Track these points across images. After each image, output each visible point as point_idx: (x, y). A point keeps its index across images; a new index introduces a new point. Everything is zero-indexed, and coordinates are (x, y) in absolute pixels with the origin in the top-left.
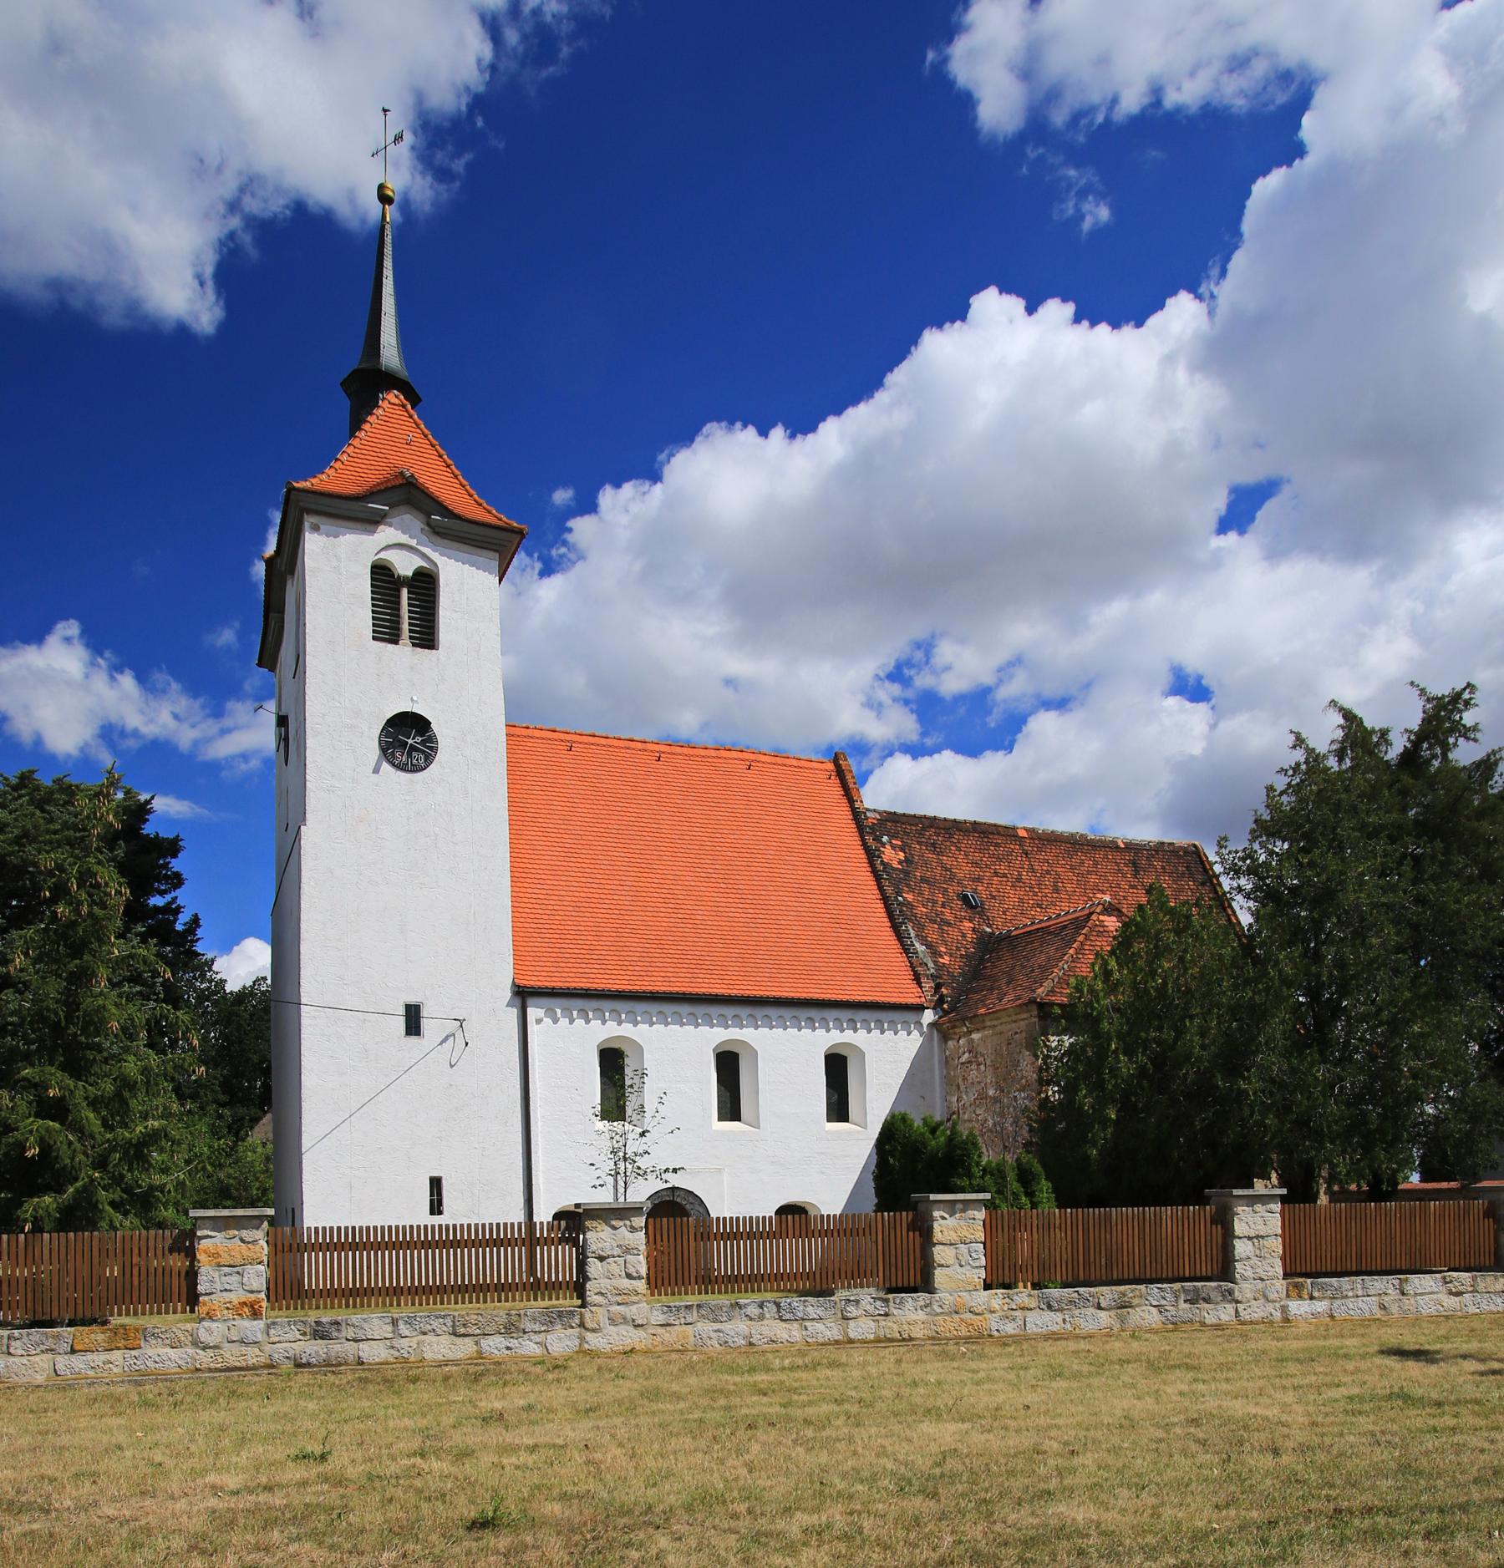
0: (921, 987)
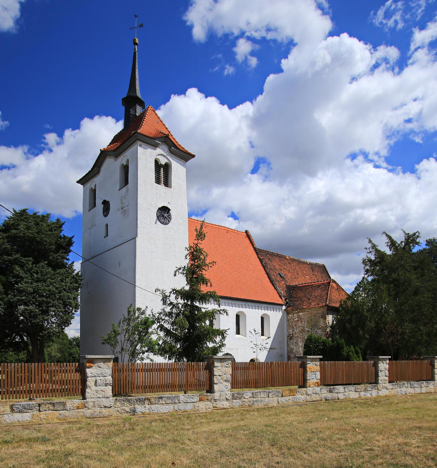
0: (282, 299)
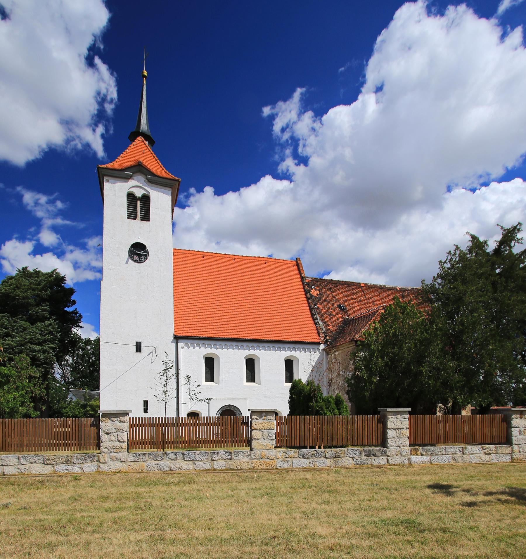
0: (320, 336)
